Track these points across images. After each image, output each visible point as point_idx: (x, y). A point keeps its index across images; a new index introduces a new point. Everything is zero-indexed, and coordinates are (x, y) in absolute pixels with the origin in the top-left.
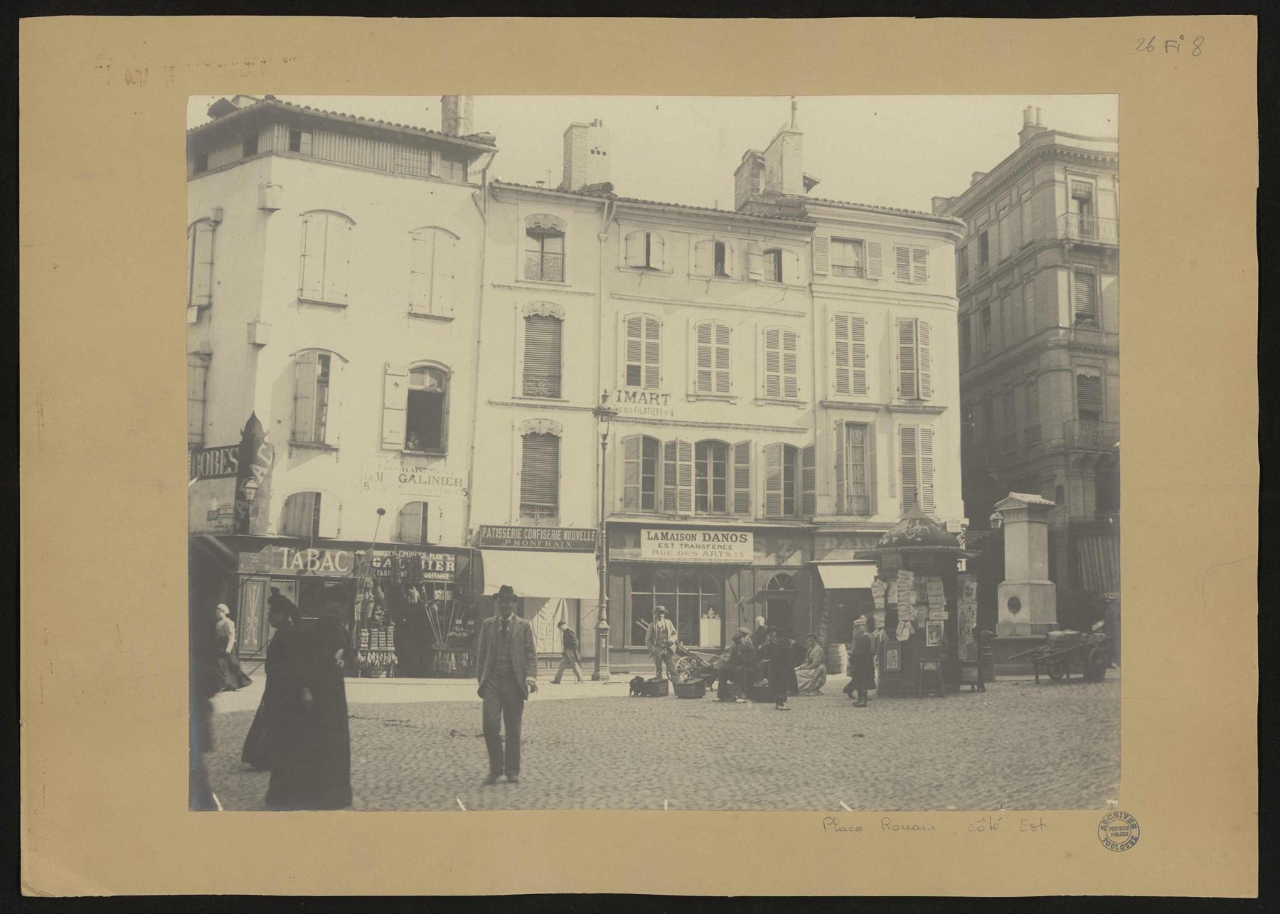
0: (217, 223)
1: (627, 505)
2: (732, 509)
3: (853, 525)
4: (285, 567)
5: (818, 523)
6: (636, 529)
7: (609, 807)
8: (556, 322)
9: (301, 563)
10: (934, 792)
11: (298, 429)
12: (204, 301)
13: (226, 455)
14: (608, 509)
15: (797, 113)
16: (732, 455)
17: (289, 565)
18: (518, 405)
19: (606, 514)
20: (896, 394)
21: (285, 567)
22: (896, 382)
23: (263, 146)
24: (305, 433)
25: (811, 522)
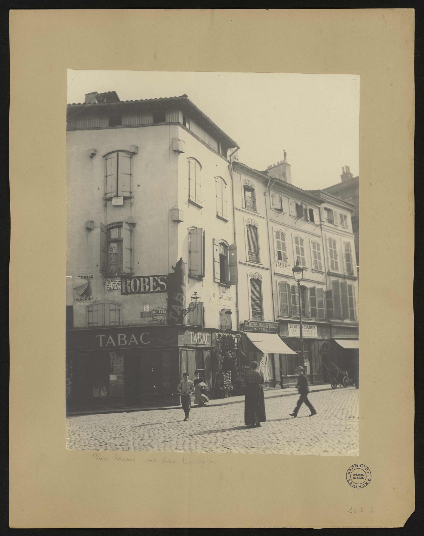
0: (134, 154)
1: (283, 312)
2: (310, 315)
3: (339, 323)
4: (192, 342)
5: (332, 322)
6: (286, 323)
7: (217, 448)
8: (255, 228)
9: (196, 340)
10: (223, 420)
11: (192, 269)
12: (127, 195)
13: (154, 280)
14: (276, 314)
15: (287, 157)
16: (308, 293)
17: (193, 342)
18: (248, 265)
19: (276, 317)
20: (345, 271)
21: (192, 342)
22: (345, 267)
23: (169, 118)
24: (197, 270)
25: (329, 321)
